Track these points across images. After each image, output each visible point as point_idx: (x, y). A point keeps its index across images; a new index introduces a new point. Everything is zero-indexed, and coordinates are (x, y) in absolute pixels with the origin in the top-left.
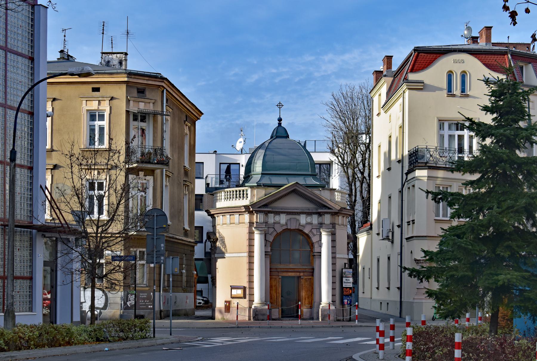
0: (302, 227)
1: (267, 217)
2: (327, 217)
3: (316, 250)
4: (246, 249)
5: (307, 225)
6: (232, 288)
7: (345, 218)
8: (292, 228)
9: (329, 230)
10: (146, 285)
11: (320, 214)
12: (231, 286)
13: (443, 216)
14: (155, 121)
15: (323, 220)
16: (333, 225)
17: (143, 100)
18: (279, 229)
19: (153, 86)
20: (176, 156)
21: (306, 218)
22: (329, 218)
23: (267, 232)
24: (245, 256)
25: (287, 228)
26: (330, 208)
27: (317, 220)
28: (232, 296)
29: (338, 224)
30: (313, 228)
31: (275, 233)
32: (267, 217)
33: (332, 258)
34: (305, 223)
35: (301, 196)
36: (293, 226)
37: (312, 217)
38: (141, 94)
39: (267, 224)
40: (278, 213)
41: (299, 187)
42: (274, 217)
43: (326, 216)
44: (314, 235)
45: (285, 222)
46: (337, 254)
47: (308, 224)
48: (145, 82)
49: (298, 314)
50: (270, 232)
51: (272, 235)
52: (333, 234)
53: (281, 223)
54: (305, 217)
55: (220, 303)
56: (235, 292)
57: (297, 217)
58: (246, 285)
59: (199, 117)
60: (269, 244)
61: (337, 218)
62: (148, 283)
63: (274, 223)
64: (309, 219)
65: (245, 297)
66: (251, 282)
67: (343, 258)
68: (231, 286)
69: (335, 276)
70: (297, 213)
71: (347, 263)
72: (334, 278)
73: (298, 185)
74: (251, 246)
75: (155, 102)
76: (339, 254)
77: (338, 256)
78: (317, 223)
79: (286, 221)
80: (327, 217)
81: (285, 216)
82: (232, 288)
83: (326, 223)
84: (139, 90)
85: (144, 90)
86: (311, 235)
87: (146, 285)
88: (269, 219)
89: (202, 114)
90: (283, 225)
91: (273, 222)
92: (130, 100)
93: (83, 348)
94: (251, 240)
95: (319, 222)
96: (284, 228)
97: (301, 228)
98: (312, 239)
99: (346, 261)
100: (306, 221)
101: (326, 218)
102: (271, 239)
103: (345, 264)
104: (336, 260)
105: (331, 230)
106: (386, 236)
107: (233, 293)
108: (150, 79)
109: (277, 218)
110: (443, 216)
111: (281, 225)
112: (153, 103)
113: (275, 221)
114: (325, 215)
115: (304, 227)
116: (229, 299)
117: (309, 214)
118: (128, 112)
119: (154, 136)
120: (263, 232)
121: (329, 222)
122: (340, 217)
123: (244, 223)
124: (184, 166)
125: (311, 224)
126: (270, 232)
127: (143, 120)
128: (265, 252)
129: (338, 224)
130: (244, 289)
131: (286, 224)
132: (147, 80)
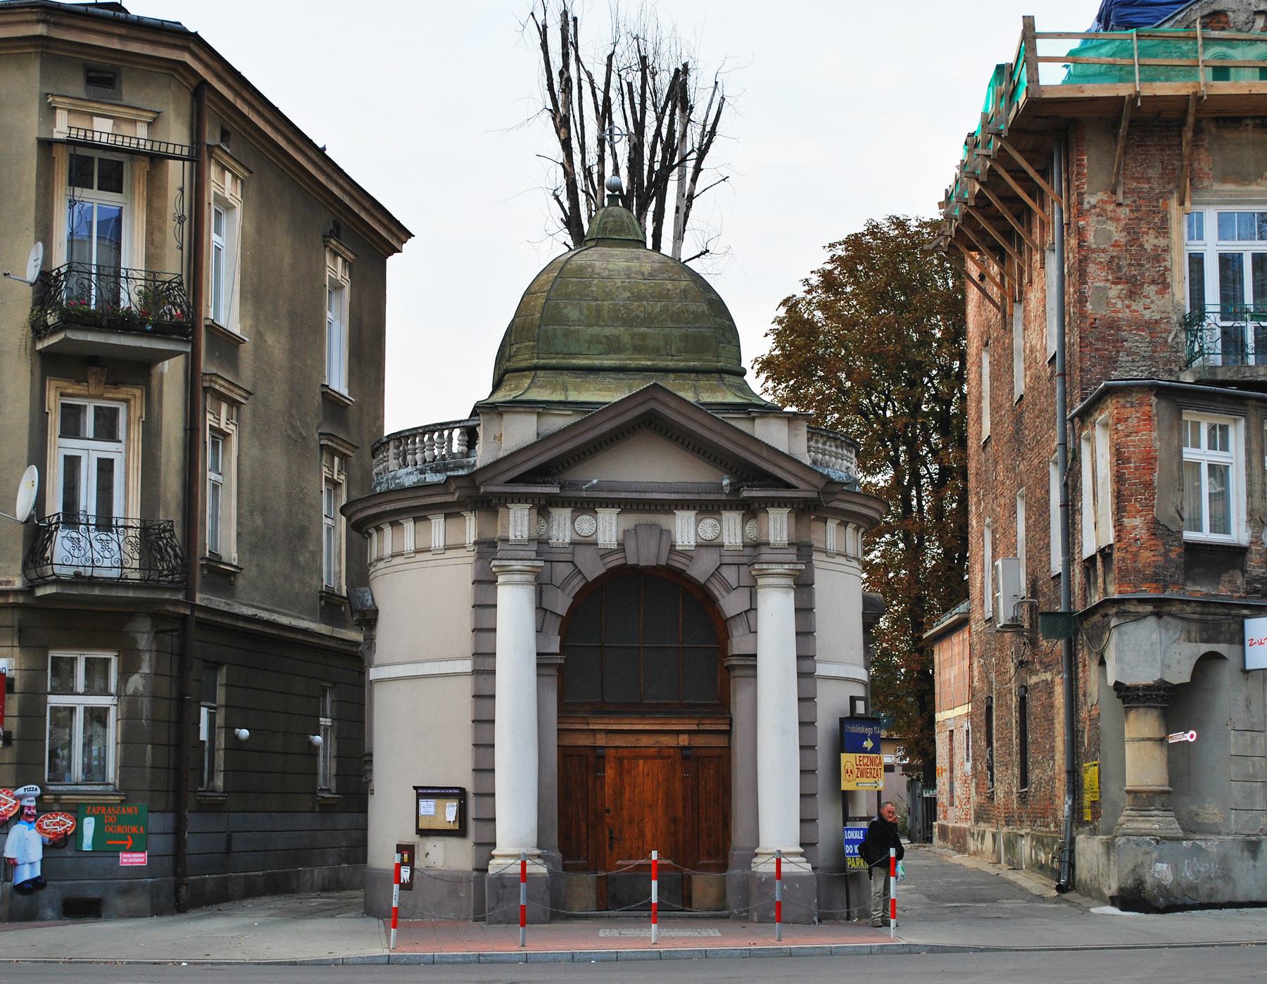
0: (685, 561)
1: (547, 522)
2: (775, 520)
3: (738, 645)
4: (465, 641)
5: (703, 551)
6: (423, 793)
7: (850, 529)
8: (643, 563)
9: (787, 566)
10: (114, 784)
11: (751, 510)
12: (415, 788)
13: (1213, 529)
14: (155, 187)
15: (760, 531)
16: (803, 550)
17: (106, 109)
18: (593, 569)
19: (141, 60)
20: (276, 344)
21: (697, 523)
22: (785, 527)
23: (545, 579)
24: (465, 674)
25: (621, 562)
26: (789, 486)
27: (739, 532)
28: (421, 826)
29: (825, 551)
30: (726, 560)
31: (577, 584)
32: (547, 522)
33: (800, 675)
34: (693, 543)
35: (676, 440)
36: (646, 555)
37: (720, 521)
38: (101, 90)
39: (545, 548)
40: (586, 505)
41: (663, 404)
42: (573, 523)
43: (771, 517)
44: (729, 589)
45: (614, 539)
46: (820, 662)
47: (703, 545)
48: (116, 45)
49: (650, 902)
50: (558, 580)
51: (567, 591)
52: (803, 586)
53: (600, 541)
54: (693, 519)
55: (382, 854)
56: (428, 807)
57: (662, 520)
58: (462, 777)
59: (395, 243)
60: (554, 626)
61: (817, 526)
62: (117, 782)
63: (574, 543)
64: (708, 529)
65: (460, 831)
66: (485, 770)
67: (846, 679)
68: (415, 788)
69: (813, 747)
70: (663, 505)
71: (860, 698)
72: (808, 752)
73: (660, 396)
74: (484, 630)
75: (155, 119)
76: (826, 662)
77: (821, 670)
78: (739, 541)
79: (621, 537)
80: (775, 520)
81: (614, 517)
82: (423, 793)
83: (772, 540)
84: (92, 74)
85: (115, 74)
86: (716, 589)
87: (114, 784)
88: (555, 527)
89: (410, 235)
90: (611, 552)
91: (568, 540)
92: (55, 108)
93: (1014, 731)
94: (485, 607)
95: (747, 541)
96: (614, 561)
97: (678, 563)
98: (721, 603)
99: (859, 691)
100: (697, 534)
101: (771, 524)
102: (561, 603)
103: (853, 700)
104: (815, 684)
105: (792, 566)
106: (1010, 617)
107: (422, 812)
108: (134, 33)
109: (585, 525)
110: (1213, 529)
111: (602, 552)
112: (149, 124)
113: (577, 538)
114: (770, 510)
115: (691, 558)
116: (410, 837)
117: (707, 507)
118: (47, 145)
119: (150, 241)
120: (531, 578)
121: (784, 539)
122: (832, 525)
123: (463, 547)
124: (324, 386)
125: (715, 545)
126: (558, 580)
127: (112, 182)
128: (538, 654)
129: (825, 551)
130: (459, 795)
131: (621, 547)
132: (121, 37)
